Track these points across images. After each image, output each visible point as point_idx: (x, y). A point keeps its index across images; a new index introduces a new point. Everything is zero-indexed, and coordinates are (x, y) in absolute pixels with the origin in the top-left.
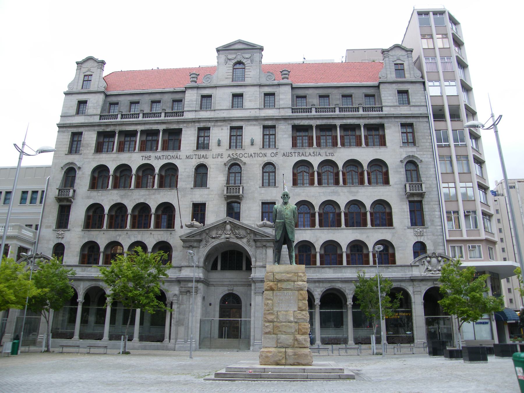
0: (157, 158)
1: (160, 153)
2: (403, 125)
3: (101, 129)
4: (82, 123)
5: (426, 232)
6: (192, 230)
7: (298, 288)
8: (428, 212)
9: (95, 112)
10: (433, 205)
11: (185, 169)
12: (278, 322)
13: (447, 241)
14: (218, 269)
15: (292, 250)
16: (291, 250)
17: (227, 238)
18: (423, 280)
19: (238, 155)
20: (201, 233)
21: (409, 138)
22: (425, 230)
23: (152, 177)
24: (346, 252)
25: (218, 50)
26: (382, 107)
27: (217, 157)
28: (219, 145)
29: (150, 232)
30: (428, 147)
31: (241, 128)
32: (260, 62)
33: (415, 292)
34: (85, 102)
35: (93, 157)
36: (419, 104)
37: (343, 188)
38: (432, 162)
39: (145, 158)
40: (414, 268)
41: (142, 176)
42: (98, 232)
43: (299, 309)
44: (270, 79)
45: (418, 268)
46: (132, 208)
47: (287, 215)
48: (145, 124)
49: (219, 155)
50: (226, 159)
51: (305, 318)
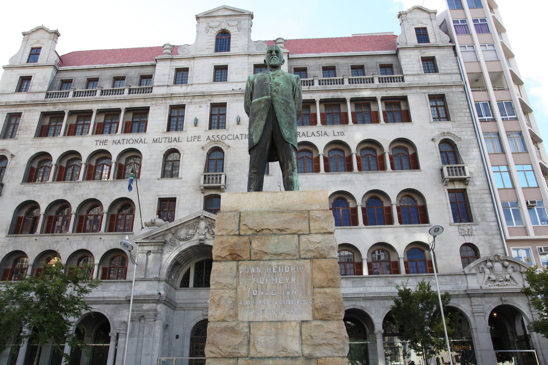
0: (115, 143)
1: (119, 136)
2: (432, 97)
3: (45, 109)
4: (21, 102)
5: (476, 230)
6: (151, 230)
7: (312, 251)
8: (475, 203)
9: (40, 89)
10: (482, 195)
11: (151, 155)
12: (252, 358)
13: (507, 241)
14: (190, 286)
15: (290, 168)
16: (288, 167)
17: (201, 240)
18: (484, 294)
19: (220, 137)
20: (164, 234)
21: (440, 112)
22: (474, 228)
23: (108, 167)
24: (367, 259)
25: (198, 18)
26: (403, 78)
27: (193, 140)
28: (196, 125)
29: (100, 236)
30: (466, 122)
31: (224, 105)
32: (250, 30)
33: (476, 313)
34: (29, 78)
35: (32, 142)
36: (450, 72)
37: (358, 175)
38: (474, 140)
39: (100, 142)
40: (469, 278)
41: (96, 167)
42: (28, 238)
43: (317, 315)
44: (261, 48)
45: (475, 277)
46: (77, 206)
47: (277, 84)
48: (102, 101)
49: (195, 137)
50: (204, 142)
51: (335, 341)
